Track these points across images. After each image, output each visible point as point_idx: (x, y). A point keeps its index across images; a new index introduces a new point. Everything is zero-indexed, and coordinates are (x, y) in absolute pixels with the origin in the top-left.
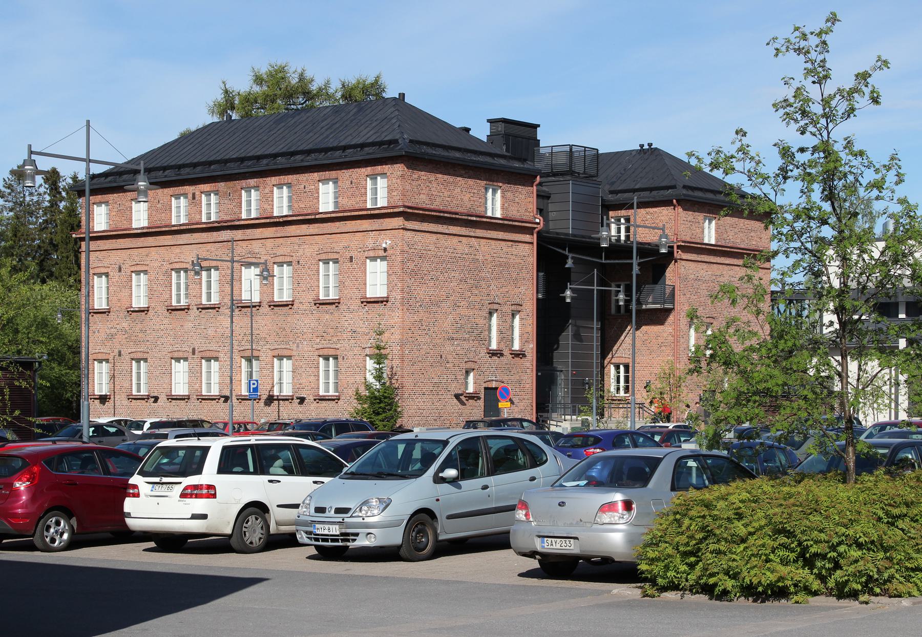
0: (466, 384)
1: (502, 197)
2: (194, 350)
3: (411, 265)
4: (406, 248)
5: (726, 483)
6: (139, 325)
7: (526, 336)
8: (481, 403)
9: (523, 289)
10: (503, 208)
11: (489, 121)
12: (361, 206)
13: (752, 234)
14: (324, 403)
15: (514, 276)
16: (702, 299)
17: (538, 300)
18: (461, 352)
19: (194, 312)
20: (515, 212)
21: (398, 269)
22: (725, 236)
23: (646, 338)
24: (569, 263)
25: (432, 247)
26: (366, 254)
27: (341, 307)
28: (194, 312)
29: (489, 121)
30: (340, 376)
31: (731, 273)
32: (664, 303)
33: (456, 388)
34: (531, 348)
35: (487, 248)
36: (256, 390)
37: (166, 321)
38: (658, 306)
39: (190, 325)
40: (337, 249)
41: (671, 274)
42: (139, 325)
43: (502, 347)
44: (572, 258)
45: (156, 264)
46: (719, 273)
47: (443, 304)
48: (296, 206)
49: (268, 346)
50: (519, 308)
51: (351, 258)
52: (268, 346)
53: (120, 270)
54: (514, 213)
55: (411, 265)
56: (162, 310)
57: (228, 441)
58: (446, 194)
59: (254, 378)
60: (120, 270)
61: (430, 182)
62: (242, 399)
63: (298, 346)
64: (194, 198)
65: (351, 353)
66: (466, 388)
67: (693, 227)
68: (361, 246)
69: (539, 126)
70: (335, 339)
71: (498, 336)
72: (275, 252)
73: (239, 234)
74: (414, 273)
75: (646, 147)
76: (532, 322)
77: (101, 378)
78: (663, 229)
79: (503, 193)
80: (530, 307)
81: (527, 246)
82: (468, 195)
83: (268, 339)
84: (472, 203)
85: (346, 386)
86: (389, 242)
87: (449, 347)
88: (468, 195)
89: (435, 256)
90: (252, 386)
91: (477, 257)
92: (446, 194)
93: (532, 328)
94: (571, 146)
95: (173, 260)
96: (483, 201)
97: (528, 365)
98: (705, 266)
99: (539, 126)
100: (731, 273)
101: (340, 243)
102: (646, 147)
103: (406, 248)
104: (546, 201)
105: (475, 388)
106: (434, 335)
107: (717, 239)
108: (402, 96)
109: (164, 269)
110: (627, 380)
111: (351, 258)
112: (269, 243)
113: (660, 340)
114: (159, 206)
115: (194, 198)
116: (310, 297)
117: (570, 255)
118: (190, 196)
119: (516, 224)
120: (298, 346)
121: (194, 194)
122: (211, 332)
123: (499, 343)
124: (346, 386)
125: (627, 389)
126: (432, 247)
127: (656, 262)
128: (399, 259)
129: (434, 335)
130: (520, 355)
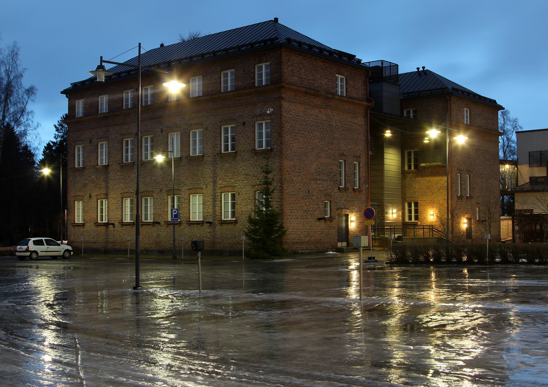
5: (11, 246)
13: (489, 121)
14: (225, 226)
20: (355, 95)
23: (429, 184)
30: (237, 207)
33: (318, 214)
36: (176, 216)
51: (244, 123)
53: (91, 142)
60: (91, 142)
61: (300, 69)
62: (168, 224)
63: (206, 187)
65: (244, 190)
75: (421, 69)
77: (79, 213)
84: (328, 86)
85: (241, 213)
90: (174, 214)
91: (331, 123)
94: (382, 62)
102: (421, 69)
108: (276, 20)
110: (416, 211)
111: (244, 123)
113: (439, 186)
120: (206, 187)
124: (241, 213)
130: (359, 190)
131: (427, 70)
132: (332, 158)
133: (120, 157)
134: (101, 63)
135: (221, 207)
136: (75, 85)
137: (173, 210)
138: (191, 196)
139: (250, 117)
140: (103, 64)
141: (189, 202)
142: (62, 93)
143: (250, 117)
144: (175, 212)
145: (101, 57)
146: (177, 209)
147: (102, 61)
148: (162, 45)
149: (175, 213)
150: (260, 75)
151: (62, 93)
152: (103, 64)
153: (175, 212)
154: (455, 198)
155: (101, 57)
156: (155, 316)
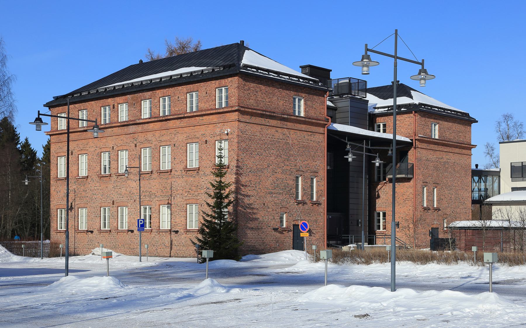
0: (282, 222)
1: (305, 104)
2: (113, 202)
3: (244, 145)
4: (240, 134)
6: (83, 188)
7: (320, 192)
8: (291, 234)
9: (318, 163)
10: (305, 111)
11: (301, 67)
12: (213, 107)
15: (312, 154)
16: (431, 172)
17: (328, 170)
18: (277, 202)
19: (114, 178)
20: (313, 114)
21: (235, 147)
22: (444, 134)
24: (348, 147)
25: (258, 134)
26: (215, 138)
27: (201, 173)
28: (114, 178)
29: (301, 67)
31: (448, 157)
32: (407, 174)
34: (324, 199)
35: (295, 136)
37: (98, 184)
38: (403, 176)
39: (111, 186)
40: (198, 136)
41: (412, 155)
42: (83, 188)
43: (305, 198)
44: (350, 145)
45: (93, 149)
46: (440, 157)
47: (265, 171)
48: (173, 110)
49: (157, 199)
50: (316, 174)
51: (206, 141)
52: (157, 199)
54: (312, 114)
55: (244, 145)
56: (95, 178)
57: (488, 223)
58: (267, 100)
59: (142, 218)
64: (114, 108)
66: (283, 225)
67: (425, 129)
68: (212, 133)
69: (331, 71)
70: (196, 193)
71: (302, 192)
72: (160, 139)
73: (139, 128)
74: (245, 150)
76: (324, 183)
78: (422, 64)
79: (305, 101)
80: (323, 174)
81: (321, 136)
82: (282, 102)
83: (157, 194)
84: (285, 106)
86: (229, 130)
87: (269, 198)
88: (282, 102)
89: (260, 140)
90: (140, 223)
92: (267, 100)
93: (324, 188)
94: (350, 79)
95: (102, 146)
96: (292, 106)
97: (322, 210)
98: (432, 152)
99: (331, 71)
100: (448, 157)
101: (200, 131)
103: (240, 134)
104: (334, 111)
105: (287, 225)
106: (259, 191)
107: (439, 136)
108: (243, 42)
109: (97, 152)
111: (206, 141)
112: (157, 134)
113: (405, 197)
114: (94, 113)
115: (114, 108)
116: (182, 167)
117: (349, 143)
118: (112, 106)
119: (314, 121)
121: (114, 106)
122: (123, 190)
123: (302, 196)
125: (384, 228)
126: (258, 134)
127: (404, 148)
128: (236, 141)
129: (259, 191)
130: (318, 204)
131: (402, 84)
132: (288, 173)
133: (99, 169)
134: (39, 116)
135: (187, 217)
136: (57, 98)
137: (140, 221)
138: (161, 206)
139: (211, 136)
140: (41, 116)
141: (159, 213)
142: (45, 106)
143: (211, 136)
144: (141, 222)
145: (39, 111)
146: (143, 220)
147: (39, 114)
148: (141, 61)
149: (142, 223)
150: (221, 98)
151: (45, 106)
152: (41, 116)
153: (141, 222)
154: (420, 208)
155: (39, 111)
156: (388, 311)
